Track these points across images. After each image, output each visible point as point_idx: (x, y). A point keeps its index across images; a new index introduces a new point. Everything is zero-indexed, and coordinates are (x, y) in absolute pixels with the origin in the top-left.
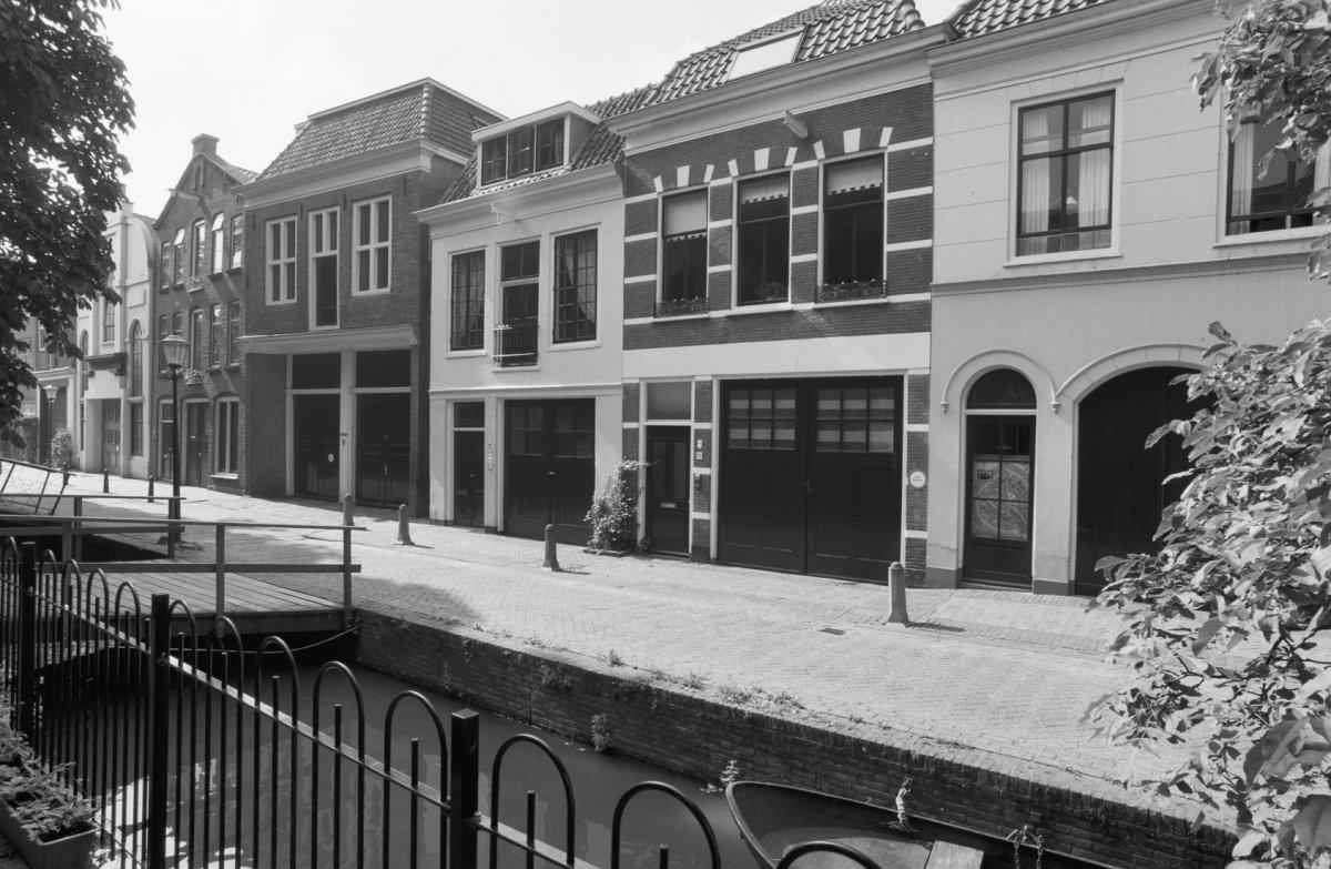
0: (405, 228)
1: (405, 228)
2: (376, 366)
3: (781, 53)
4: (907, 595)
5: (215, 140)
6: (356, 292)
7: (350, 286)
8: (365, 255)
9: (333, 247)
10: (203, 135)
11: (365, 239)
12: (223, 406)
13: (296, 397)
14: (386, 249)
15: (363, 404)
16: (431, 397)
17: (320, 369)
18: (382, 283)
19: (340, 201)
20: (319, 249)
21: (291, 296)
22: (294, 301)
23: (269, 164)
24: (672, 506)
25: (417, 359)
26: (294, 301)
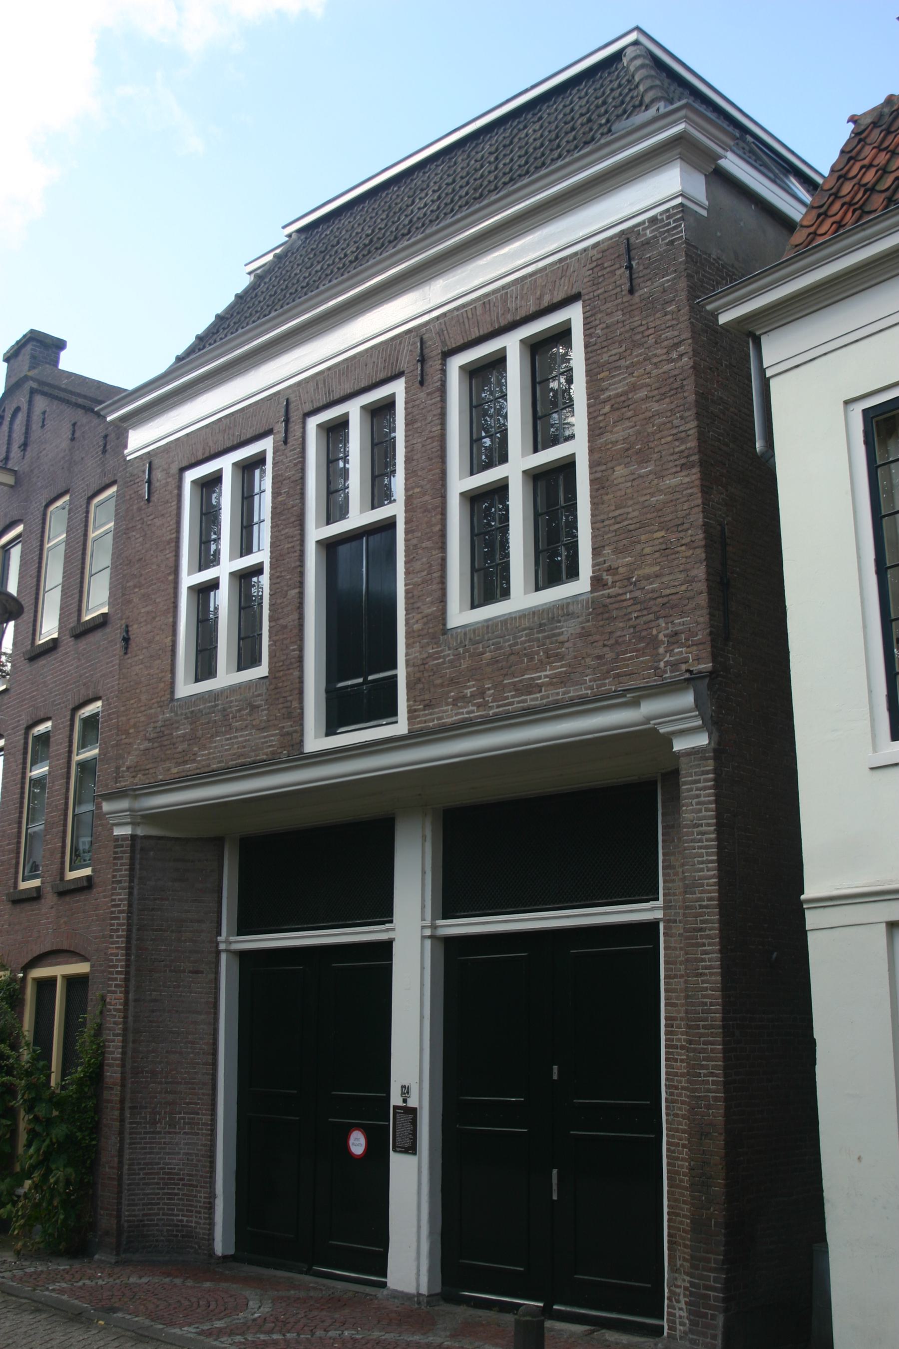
0: (634, 388)
1: (634, 388)
2: (505, 835)
3: (214, 502)
4: (814, 941)
5: (60, 345)
6: (460, 615)
7: (442, 599)
8: (487, 504)
9: (379, 494)
10: (32, 331)
11: (488, 449)
12: (46, 986)
13: (248, 960)
14: (567, 466)
15: (458, 962)
16: (812, 919)
17: (320, 858)
18: (554, 564)
19: (407, 361)
20: (334, 508)
21: (247, 656)
22: (262, 671)
23: (190, 340)
24: (775, 954)
25: (708, 796)
26: (262, 671)
